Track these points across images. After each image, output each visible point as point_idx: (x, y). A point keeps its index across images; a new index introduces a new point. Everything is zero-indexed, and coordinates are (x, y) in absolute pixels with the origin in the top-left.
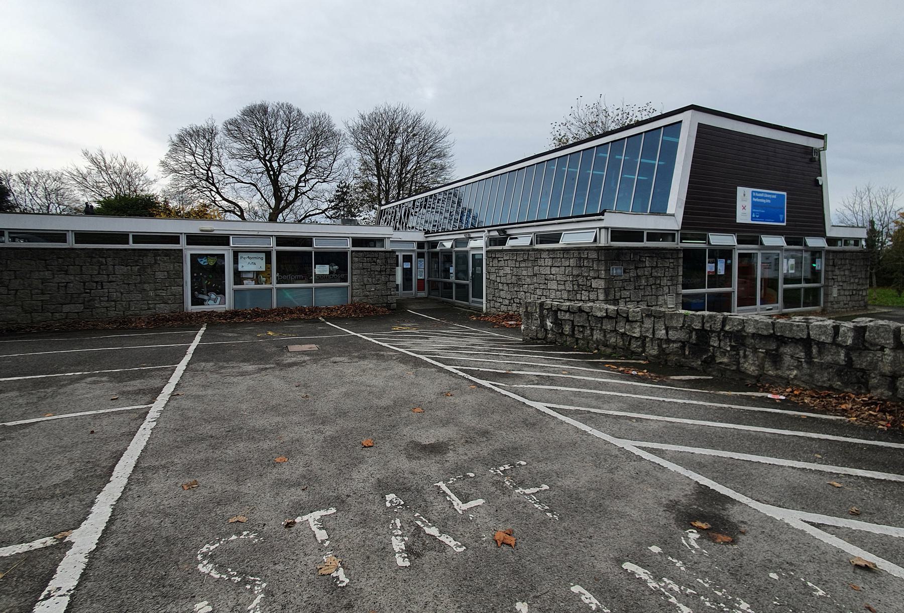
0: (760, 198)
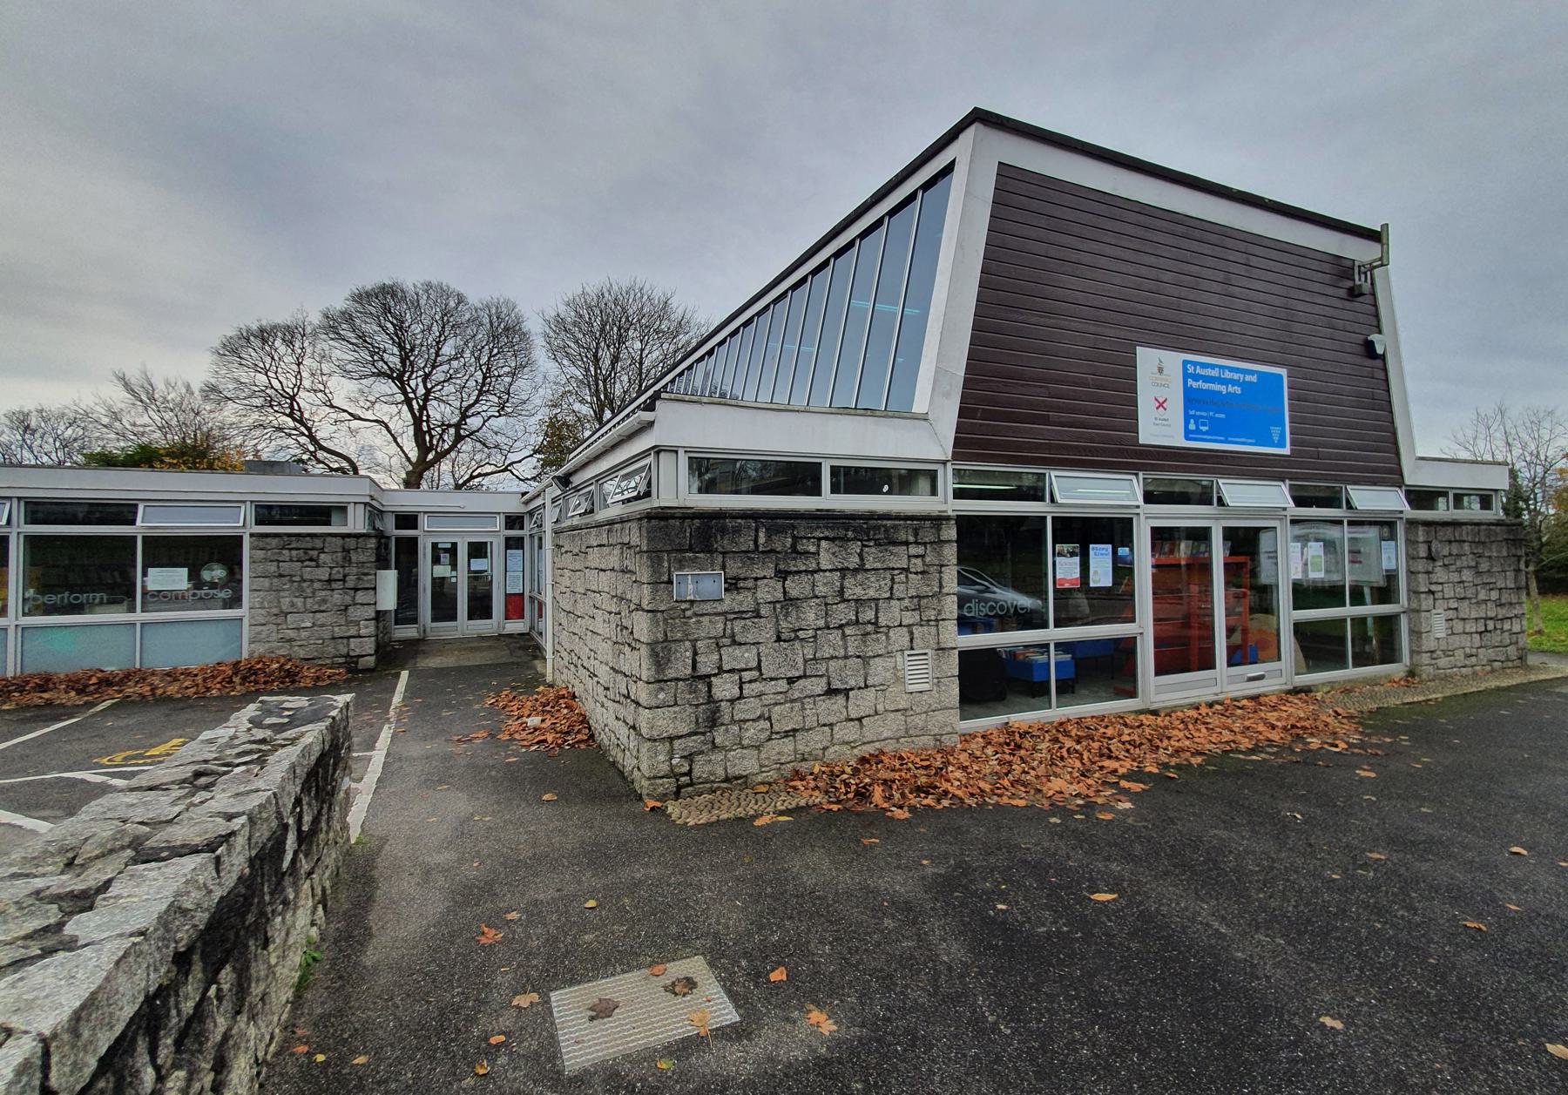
0: (1207, 379)
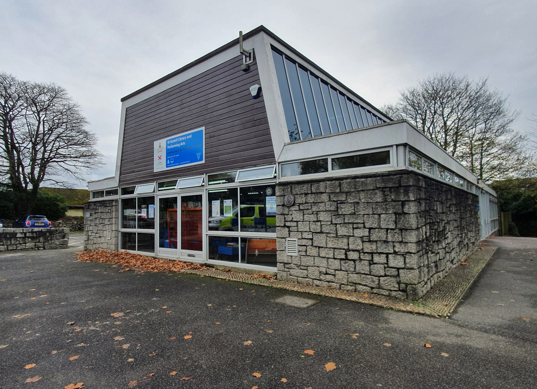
0: (175, 143)
